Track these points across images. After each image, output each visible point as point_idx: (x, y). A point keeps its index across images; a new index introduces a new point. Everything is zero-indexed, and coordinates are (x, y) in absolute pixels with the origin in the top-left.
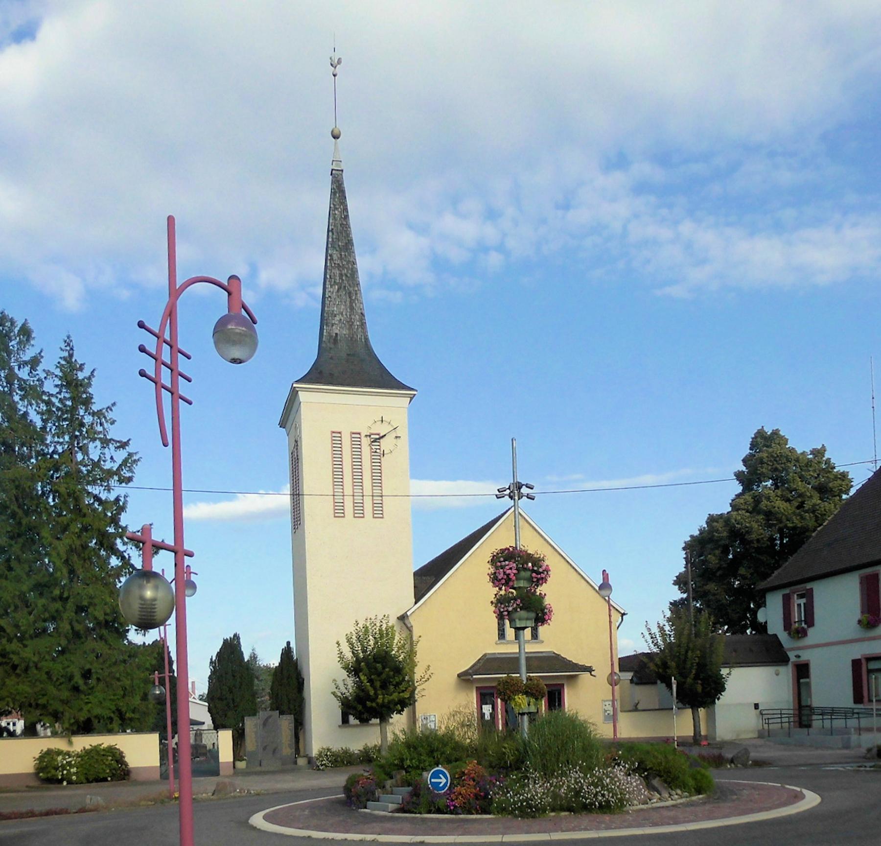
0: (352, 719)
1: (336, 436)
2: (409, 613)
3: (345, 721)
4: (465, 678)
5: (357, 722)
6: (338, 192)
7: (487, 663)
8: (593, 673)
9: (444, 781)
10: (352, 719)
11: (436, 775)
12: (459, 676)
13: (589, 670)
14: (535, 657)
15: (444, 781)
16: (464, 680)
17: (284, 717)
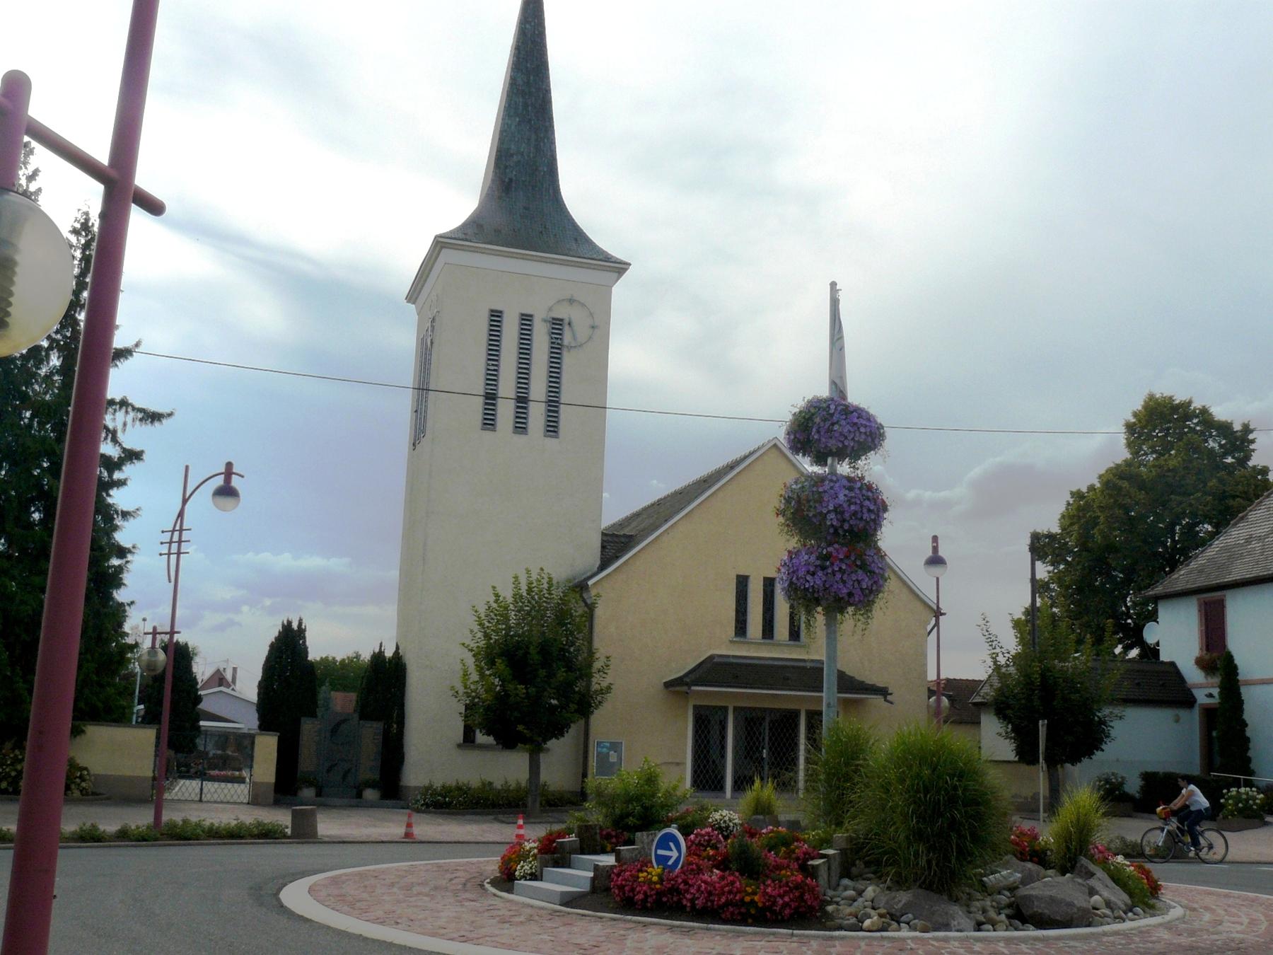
0: (481, 738)
1: (496, 317)
2: (590, 583)
3: (469, 738)
4: (678, 686)
5: (490, 740)
6: (835, 303)
7: (715, 671)
8: (889, 698)
9: (675, 854)
10: (481, 738)
11: (665, 842)
12: (668, 685)
13: (883, 692)
14: (793, 667)
15: (675, 854)
16: (674, 692)
17: (368, 724)
